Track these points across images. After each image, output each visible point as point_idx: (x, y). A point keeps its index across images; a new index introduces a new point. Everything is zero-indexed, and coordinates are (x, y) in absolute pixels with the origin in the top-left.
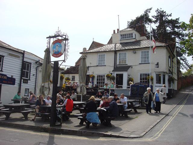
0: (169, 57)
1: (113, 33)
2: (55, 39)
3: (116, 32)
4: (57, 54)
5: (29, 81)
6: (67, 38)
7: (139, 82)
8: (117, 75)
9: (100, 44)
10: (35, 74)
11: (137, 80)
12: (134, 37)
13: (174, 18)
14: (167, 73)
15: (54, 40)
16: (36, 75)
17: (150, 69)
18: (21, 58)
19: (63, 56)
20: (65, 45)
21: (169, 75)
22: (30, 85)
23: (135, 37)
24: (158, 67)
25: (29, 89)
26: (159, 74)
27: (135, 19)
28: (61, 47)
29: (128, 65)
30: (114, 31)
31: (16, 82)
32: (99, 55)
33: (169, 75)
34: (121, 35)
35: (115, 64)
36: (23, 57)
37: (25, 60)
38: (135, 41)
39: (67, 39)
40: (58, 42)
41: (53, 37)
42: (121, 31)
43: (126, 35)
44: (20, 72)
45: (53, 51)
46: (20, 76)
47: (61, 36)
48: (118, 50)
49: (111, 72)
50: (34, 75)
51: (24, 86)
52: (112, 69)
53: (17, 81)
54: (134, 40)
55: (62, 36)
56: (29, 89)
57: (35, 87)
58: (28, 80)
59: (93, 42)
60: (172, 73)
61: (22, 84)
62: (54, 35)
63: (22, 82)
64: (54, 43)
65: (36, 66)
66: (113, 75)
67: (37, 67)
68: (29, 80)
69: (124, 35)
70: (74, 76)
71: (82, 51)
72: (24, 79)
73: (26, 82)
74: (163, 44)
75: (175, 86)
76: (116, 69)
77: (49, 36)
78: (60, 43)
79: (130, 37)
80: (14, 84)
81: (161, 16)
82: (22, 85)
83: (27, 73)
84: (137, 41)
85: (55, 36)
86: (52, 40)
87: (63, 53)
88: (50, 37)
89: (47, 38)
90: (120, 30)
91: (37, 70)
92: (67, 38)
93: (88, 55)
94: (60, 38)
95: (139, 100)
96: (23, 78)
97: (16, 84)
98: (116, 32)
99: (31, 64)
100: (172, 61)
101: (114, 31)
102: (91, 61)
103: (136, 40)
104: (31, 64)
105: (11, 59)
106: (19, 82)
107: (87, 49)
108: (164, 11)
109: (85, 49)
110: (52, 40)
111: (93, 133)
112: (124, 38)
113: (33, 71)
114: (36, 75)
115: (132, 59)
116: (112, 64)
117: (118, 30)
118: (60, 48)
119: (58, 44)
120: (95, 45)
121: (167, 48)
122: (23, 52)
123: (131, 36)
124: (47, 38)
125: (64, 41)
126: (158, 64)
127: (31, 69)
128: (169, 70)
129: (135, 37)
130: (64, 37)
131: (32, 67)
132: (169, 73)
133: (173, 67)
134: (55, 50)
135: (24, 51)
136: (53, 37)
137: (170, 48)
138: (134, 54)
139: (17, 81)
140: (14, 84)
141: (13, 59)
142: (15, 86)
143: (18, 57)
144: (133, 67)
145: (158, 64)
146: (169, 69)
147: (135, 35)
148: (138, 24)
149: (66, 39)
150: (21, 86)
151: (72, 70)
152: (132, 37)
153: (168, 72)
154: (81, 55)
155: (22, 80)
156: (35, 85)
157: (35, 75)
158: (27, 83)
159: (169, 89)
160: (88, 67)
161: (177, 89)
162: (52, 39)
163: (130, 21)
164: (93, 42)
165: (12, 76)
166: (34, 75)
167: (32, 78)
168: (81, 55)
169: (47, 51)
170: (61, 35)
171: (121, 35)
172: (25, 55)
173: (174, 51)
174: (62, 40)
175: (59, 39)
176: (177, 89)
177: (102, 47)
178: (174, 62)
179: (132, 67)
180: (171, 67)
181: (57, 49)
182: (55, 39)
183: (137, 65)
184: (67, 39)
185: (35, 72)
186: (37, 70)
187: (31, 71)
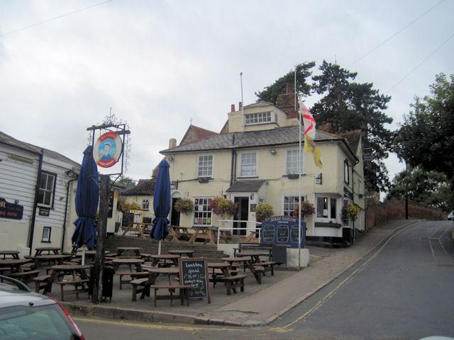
0: (346, 162)
1: (230, 110)
2: (104, 131)
3: (237, 109)
4: (108, 161)
5: (51, 212)
6: (126, 129)
7: (283, 214)
8: (236, 199)
9: (208, 131)
10: (65, 196)
11: (279, 210)
12: (273, 120)
13: (359, 81)
14: (339, 196)
15: (102, 134)
16: (67, 198)
17: (307, 189)
18: (36, 164)
19: (118, 165)
20: (123, 145)
21: (345, 199)
22: (54, 219)
23: (276, 120)
24: (321, 183)
25: (50, 228)
26: (324, 198)
27: (275, 82)
28: (114, 146)
29: (260, 179)
30: (233, 107)
31: (24, 212)
32: (201, 159)
33: (345, 199)
34: (247, 116)
35: (232, 175)
36: (41, 162)
37: (44, 167)
38: (276, 129)
39: (128, 132)
40: (109, 137)
41: (100, 128)
42: (246, 108)
43: (256, 115)
44: (34, 192)
45: (99, 155)
46: (33, 201)
47: (115, 126)
48: (238, 148)
49: (225, 193)
50: (61, 199)
51: (41, 222)
52: (227, 186)
53: (27, 212)
54: (273, 127)
55: (117, 127)
56: (50, 228)
57: (63, 223)
58: (49, 209)
59: (192, 128)
60: (351, 196)
61: (38, 218)
62: (101, 124)
63: (37, 214)
64: (103, 138)
65: (67, 181)
66: (228, 198)
67: (68, 183)
68: (53, 208)
69: (252, 115)
70: (147, 201)
71: (166, 147)
72: (41, 207)
73: (45, 212)
74: (332, 136)
75: (360, 224)
76: (235, 185)
77: (91, 126)
78: (113, 138)
79: (265, 120)
80: (19, 217)
81: (333, 75)
82: (36, 218)
83: (381, 174)
84: (280, 128)
85: (104, 126)
86: (98, 133)
87: (118, 158)
88: (94, 128)
89: (88, 129)
90: (245, 104)
91: (68, 189)
92: (126, 129)
93: (178, 159)
94: (114, 129)
95: (268, 253)
96: (39, 204)
97: (24, 216)
98: (237, 109)
99: (56, 175)
100: (353, 171)
101: (233, 107)
102: (184, 170)
103: (277, 127)
104: (56, 175)
105: (14, 165)
106: (31, 214)
107: (178, 144)
108: (340, 68)
109: (173, 141)
110: (98, 133)
111: (175, 317)
112: (252, 121)
113: (60, 191)
114: (67, 198)
115: (265, 166)
116: (228, 177)
117: (240, 104)
118: (113, 149)
119: (108, 141)
120: (196, 133)
121: (339, 144)
122: (40, 152)
123: (254, 118)
124: (88, 129)
125: (122, 136)
126: (320, 178)
127: (57, 186)
128: (345, 190)
129: (276, 120)
130: (122, 127)
131: (57, 182)
132: (345, 196)
133: (353, 183)
134: (102, 152)
135: (43, 150)
136: (100, 128)
137: (346, 144)
138: (273, 156)
139: (27, 212)
140: (19, 217)
141: (19, 166)
142: (22, 221)
143: (30, 162)
144: (271, 183)
145: (320, 178)
146: (345, 188)
147: (276, 116)
148: (282, 93)
149: (125, 132)
150: (35, 222)
151: (143, 189)
152: (269, 119)
153: (342, 193)
154: (162, 157)
155: (38, 210)
156: (63, 219)
157: (65, 200)
158: (48, 215)
159: (247, 220)
160: (178, 182)
161: (363, 229)
162: (97, 131)
163: (277, 79)
164: (192, 128)
165: (16, 201)
166: (61, 199)
167: (59, 206)
168: (162, 157)
169: (89, 153)
170: (115, 123)
171: (247, 116)
172: (45, 159)
173: (356, 150)
174: (119, 133)
175: (111, 132)
176: (363, 229)
177: (207, 140)
178: (356, 173)
179: (267, 184)
180: (351, 183)
181: (107, 151)
182: (104, 131)
183: (277, 177)
184: (128, 132)
185: (66, 192)
186: (68, 189)
187: (56, 190)
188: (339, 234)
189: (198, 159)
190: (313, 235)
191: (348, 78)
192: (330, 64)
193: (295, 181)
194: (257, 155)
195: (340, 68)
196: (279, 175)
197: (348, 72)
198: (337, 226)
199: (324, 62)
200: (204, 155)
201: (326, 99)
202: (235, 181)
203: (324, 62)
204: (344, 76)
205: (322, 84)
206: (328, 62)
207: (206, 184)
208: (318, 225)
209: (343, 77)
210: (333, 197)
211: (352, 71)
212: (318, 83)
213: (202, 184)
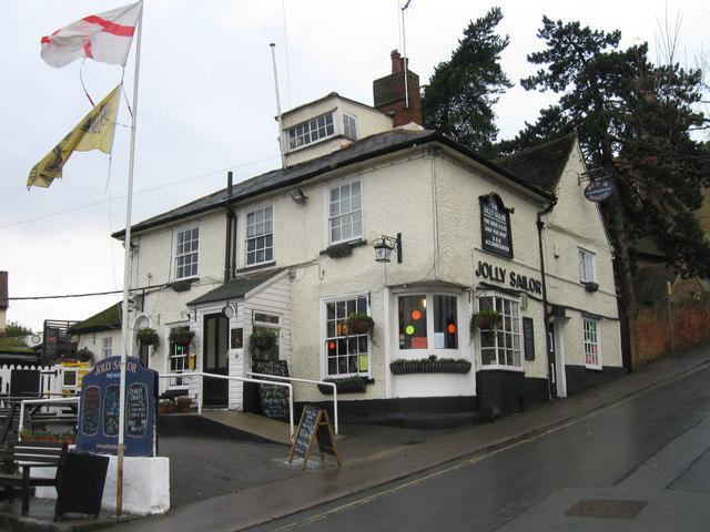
12: (339, 128)
54: (345, 143)
69: (299, 127)
79: (322, 135)
89: (399, 235)
108: (582, 28)
116: (220, 274)
124: (399, 235)
152: (331, 130)
153: (473, 281)
161: (618, 363)
176: (618, 363)
183: (310, 259)
188: (465, 387)
189: (175, 238)
190: (388, 396)
191: (604, 47)
192: (560, 23)
193: (344, 262)
194: (275, 218)
195: (582, 28)
196: (313, 254)
197: (602, 34)
198: (460, 368)
199: (546, 20)
200: (184, 229)
201: (567, 102)
202: (234, 276)
203: (546, 20)
204: (596, 44)
205: (557, 69)
206: (554, 18)
207: (186, 293)
208: (400, 368)
209: (591, 46)
210: (405, 293)
211: (609, 30)
212: (546, 67)
213: (182, 293)
